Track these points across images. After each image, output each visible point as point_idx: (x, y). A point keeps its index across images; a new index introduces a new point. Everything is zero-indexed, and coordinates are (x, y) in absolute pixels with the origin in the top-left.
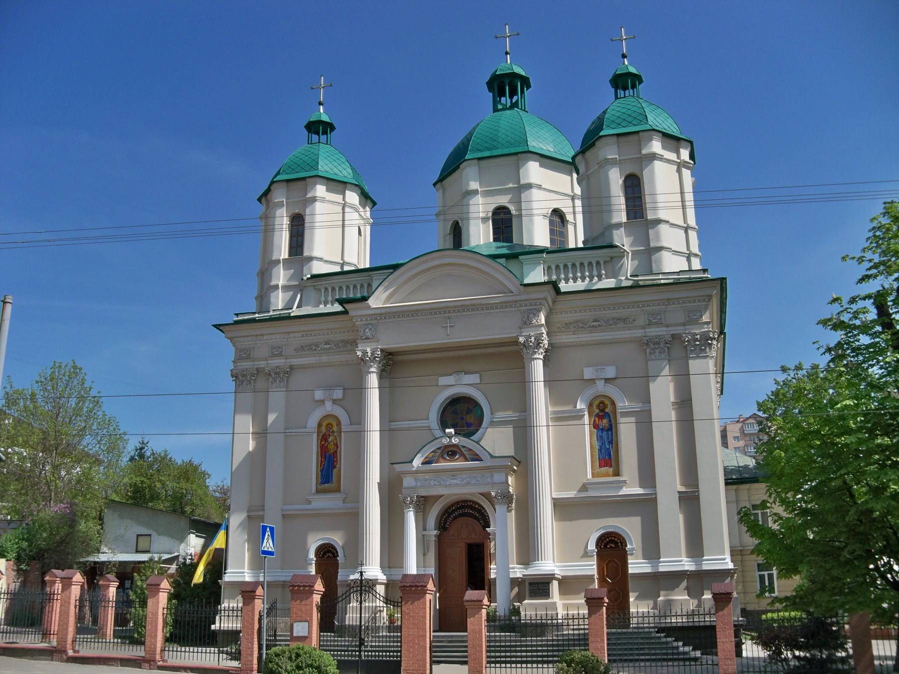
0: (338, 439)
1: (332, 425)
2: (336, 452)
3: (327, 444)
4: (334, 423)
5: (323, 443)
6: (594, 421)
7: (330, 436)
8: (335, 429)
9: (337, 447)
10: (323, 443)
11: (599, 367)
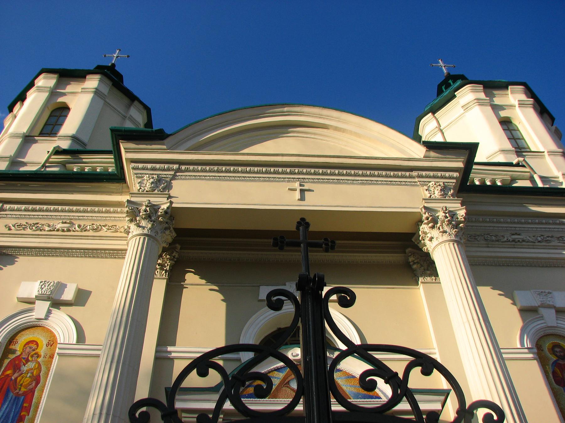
0: (43, 368)
1: (37, 344)
2: (32, 391)
3: (16, 375)
4: (43, 340)
5: (9, 372)
6: (554, 373)
7: (27, 361)
8: (43, 350)
9: (38, 383)
10: (9, 372)
11: (543, 291)
